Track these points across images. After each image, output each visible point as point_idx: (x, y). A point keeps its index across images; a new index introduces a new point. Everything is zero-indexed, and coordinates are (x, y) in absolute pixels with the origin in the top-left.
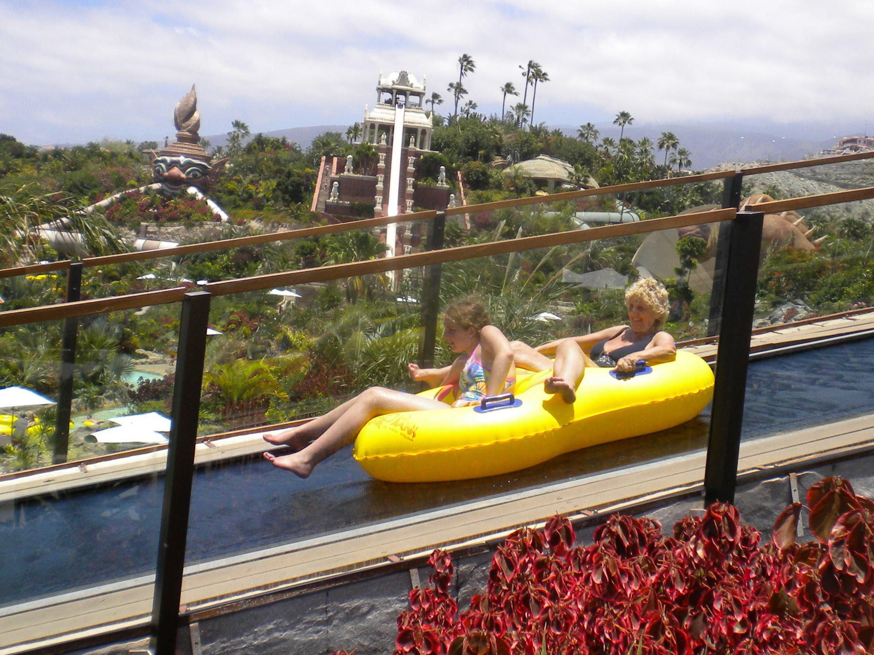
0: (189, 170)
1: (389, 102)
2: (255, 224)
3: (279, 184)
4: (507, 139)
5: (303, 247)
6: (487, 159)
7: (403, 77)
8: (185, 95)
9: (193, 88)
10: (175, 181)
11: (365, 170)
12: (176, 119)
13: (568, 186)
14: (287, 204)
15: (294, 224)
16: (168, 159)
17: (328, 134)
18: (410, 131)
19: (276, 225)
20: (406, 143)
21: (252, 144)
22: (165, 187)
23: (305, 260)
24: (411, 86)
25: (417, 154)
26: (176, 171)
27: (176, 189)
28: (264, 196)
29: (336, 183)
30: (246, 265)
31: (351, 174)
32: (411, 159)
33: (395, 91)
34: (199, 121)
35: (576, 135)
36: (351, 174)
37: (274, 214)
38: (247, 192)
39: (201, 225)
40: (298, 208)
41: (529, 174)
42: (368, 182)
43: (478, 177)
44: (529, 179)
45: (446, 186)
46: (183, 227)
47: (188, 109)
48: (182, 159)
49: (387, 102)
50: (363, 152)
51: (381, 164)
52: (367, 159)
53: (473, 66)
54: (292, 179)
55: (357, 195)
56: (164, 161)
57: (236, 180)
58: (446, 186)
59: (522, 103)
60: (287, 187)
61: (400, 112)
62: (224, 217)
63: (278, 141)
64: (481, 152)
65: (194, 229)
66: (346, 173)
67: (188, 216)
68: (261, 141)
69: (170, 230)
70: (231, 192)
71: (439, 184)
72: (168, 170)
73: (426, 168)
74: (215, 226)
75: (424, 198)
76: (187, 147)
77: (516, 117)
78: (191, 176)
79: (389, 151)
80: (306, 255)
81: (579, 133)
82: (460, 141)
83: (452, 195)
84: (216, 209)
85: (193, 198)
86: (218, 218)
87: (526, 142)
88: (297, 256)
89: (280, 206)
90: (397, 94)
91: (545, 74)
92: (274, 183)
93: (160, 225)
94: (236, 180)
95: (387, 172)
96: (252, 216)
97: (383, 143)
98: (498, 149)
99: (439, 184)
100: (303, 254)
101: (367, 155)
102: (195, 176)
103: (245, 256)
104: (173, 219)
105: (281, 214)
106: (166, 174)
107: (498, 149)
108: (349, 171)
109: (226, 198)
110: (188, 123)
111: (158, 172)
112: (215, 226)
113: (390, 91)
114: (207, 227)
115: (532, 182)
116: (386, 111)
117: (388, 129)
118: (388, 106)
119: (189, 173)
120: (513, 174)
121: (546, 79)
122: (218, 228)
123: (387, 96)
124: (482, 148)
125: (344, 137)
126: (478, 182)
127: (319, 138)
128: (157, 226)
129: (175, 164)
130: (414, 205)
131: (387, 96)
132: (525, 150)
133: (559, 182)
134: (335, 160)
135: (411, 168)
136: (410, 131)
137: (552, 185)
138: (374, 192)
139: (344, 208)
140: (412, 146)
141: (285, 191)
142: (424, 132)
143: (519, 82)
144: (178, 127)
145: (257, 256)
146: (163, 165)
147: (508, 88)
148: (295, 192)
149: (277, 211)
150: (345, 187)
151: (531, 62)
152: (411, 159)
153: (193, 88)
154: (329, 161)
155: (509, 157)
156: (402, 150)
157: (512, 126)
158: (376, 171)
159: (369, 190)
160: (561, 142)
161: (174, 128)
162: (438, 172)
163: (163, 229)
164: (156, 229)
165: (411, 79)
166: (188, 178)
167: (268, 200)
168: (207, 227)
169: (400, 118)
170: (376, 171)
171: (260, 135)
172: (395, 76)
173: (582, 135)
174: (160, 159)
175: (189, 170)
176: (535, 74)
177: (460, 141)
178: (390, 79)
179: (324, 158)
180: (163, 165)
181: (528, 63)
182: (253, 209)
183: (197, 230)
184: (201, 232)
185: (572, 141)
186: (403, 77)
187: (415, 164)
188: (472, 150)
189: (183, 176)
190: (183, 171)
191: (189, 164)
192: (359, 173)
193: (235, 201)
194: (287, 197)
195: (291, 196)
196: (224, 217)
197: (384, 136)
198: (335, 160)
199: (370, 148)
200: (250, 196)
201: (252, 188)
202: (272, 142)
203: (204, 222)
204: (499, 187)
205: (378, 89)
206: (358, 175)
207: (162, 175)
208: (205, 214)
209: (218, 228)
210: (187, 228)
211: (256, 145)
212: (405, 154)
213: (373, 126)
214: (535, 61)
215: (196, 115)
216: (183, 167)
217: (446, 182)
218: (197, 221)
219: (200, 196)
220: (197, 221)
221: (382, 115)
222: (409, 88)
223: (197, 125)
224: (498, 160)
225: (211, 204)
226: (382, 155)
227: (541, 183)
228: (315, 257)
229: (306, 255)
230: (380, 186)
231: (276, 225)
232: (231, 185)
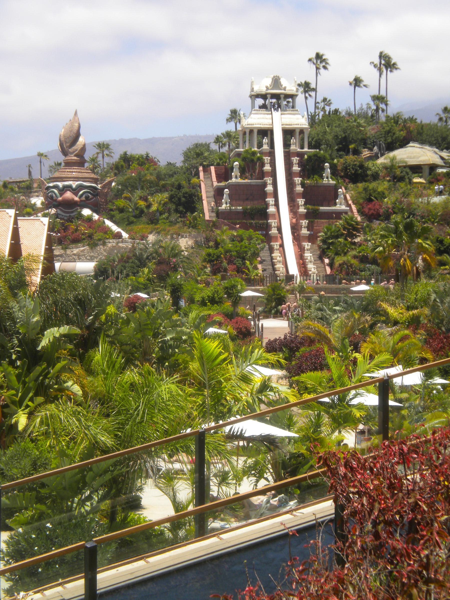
0: (81, 192)
1: (264, 107)
2: (151, 238)
3: (171, 198)
4: (371, 131)
5: (209, 255)
6: (356, 152)
7: (276, 82)
8: (68, 122)
9: (76, 113)
10: (69, 205)
11: (251, 175)
12: (61, 145)
13: (444, 170)
14: (183, 215)
15: (193, 233)
16: (60, 184)
17: (197, 146)
18: (288, 133)
19: (175, 236)
20: (286, 145)
21: (119, 163)
22: (59, 212)
23: (212, 266)
24: (285, 89)
25: (300, 155)
26: (68, 195)
27: (72, 212)
28: (158, 210)
29: (226, 190)
30: (168, 275)
31: (239, 180)
32: (295, 160)
33: (269, 96)
34: (84, 145)
35: (435, 120)
36: (239, 180)
37: (170, 226)
38: (137, 209)
39: (104, 244)
40: (195, 219)
41: (406, 162)
42: (257, 186)
43: (356, 170)
44: (405, 167)
45: (332, 182)
46: (87, 247)
47: (73, 135)
48: (74, 184)
49: (260, 107)
50: (240, 159)
51: (267, 168)
52: (253, 165)
53: (327, 63)
54: (183, 191)
55: (247, 199)
56: (56, 187)
57: (126, 198)
58: (332, 182)
59: (376, 93)
60: (179, 199)
61: (277, 114)
62: (125, 235)
63: (142, 156)
64: (352, 146)
65: (98, 248)
66: (234, 180)
67: (90, 236)
68: (127, 159)
69: (75, 251)
70: (121, 210)
71: (325, 181)
72: (61, 195)
73: (311, 167)
74: (117, 243)
75: (314, 201)
76: (75, 172)
77: (374, 107)
78: (83, 198)
79: (272, 154)
80: (213, 261)
81: (438, 118)
82: (329, 137)
83: (340, 190)
84: (115, 228)
85: (89, 219)
86: (118, 236)
87: (389, 132)
88: (204, 264)
89: (173, 217)
90: (275, 100)
91: (394, 64)
92: (166, 195)
93: (65, 248)
94: (126, 198)
95: (273, 174)
96: (149, 230)
97: (266, 147)
98: (365, 142)
99: (325, 181)
100: (210, 261)
101: (252, 160)
102: (87, 198)
103: (164, 267)
104: (76, 241)
105: (178, 226)
106: (60, 199)
107: (365, 142)
108: (236, 177)
109: (118, 216)
110: (75, 148)
111: (52, 197)
112: (117, 243)
113: (264, 97)
114: (109, 245)
115: (408, 170)
116: (262, 116)
117: (266, 133)
118: (263, 111)
119: (82, 195)
120: (390, 164)
121: (396, 69)
122: (120, 245)
123: (260, 101)
124: (351, 143)
125: (214, 147)
126: (356, 175)
127: (189, 150)
128: (62, 249)
129: (69, 188)
130: (305, 204)
131: (260, 101)
132: (389, 140)
133: (433, 167)
134: (212, 168)
135: (296, 168)
136: (288, 133)
137: (426, 171)
138: (264, 195)
139: (237, 213)
140: (293, 147)
141: (179, 203)
142: (302, 131)
143: (370, 76)
144: (65, 152)
145: (175, 266)
146: (56, 191)
147: (357, 82)
148: (186, 204)
149: (173, 223)
150: (238, 193)
151: (381, 53)
152: (295, 160)
153: (76, 113)
154: (206, 170)
155: (376, 148)
156: (285, 152)
157: (373, 118)
158: (262, 175)
159: (261, 194)
160: (422, 128)
161: (61, 154)
162: (323, 169)
163: (68, 252)
164: (62, 252)
165: (284, 82)
166: (81, 201)
167: (161, 214)
168: (109, 245)
169: (278, 121)
170: (262, 175)
171: (125, 154)
172: (268, 82)
173: (441, 119)
174: (51, 185)
175: (81, 192)
176: (387, 64)
177: (329, 137)
178: (263, 85)
179: (201, 168)
180: (56, 191)
181: (378, 54)
182: (148, 224)
183: (100, 248)
184: (105, 250)
185: (430, 126)
186: (276, 82)
187: (300, 164)
188: (344, 145)
189: (77, 199)
190: (76, 194)
191: (81, 187)
192: (246, 178)
193: (128, 218)
194: (181, 208)
195: (184, 207)
196: (125, 235)
197: (265, 140)
198: (212, 168)
199: (254, 153)
200: (142, 212)
201: (142, 203)
202: (138, 159)
203: (107, 241)
204: (375, 177)
205: (251, 96)
206: (246, 181)
207: (56, 200)
208: (106, 233)
209: (120, 245)
210: (92, 248)
211: (122, 163)
212: (288, 156)
213: (251, 131)
214: (321, 53)
215: (81, 140)
216: (75, 191)
217: (331, 178)
218: (100, 240)
219: (96, 217)
220: (100, 240)
221: (257, 120)
222: (282, 91)
223: (83, 149)
224: (366, 153)
225: (108, 223)
226: (267, 159)
227: (416, 169)
228: (222, 262)
229: (213, 261)
230: (269, 188)
231: (175, 236)
232: (121, 203)
